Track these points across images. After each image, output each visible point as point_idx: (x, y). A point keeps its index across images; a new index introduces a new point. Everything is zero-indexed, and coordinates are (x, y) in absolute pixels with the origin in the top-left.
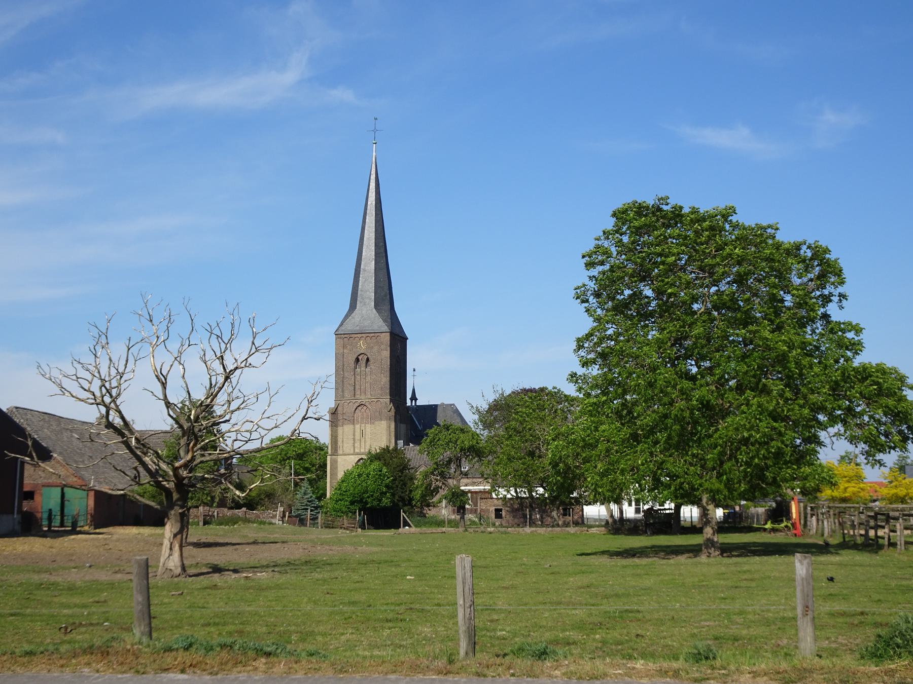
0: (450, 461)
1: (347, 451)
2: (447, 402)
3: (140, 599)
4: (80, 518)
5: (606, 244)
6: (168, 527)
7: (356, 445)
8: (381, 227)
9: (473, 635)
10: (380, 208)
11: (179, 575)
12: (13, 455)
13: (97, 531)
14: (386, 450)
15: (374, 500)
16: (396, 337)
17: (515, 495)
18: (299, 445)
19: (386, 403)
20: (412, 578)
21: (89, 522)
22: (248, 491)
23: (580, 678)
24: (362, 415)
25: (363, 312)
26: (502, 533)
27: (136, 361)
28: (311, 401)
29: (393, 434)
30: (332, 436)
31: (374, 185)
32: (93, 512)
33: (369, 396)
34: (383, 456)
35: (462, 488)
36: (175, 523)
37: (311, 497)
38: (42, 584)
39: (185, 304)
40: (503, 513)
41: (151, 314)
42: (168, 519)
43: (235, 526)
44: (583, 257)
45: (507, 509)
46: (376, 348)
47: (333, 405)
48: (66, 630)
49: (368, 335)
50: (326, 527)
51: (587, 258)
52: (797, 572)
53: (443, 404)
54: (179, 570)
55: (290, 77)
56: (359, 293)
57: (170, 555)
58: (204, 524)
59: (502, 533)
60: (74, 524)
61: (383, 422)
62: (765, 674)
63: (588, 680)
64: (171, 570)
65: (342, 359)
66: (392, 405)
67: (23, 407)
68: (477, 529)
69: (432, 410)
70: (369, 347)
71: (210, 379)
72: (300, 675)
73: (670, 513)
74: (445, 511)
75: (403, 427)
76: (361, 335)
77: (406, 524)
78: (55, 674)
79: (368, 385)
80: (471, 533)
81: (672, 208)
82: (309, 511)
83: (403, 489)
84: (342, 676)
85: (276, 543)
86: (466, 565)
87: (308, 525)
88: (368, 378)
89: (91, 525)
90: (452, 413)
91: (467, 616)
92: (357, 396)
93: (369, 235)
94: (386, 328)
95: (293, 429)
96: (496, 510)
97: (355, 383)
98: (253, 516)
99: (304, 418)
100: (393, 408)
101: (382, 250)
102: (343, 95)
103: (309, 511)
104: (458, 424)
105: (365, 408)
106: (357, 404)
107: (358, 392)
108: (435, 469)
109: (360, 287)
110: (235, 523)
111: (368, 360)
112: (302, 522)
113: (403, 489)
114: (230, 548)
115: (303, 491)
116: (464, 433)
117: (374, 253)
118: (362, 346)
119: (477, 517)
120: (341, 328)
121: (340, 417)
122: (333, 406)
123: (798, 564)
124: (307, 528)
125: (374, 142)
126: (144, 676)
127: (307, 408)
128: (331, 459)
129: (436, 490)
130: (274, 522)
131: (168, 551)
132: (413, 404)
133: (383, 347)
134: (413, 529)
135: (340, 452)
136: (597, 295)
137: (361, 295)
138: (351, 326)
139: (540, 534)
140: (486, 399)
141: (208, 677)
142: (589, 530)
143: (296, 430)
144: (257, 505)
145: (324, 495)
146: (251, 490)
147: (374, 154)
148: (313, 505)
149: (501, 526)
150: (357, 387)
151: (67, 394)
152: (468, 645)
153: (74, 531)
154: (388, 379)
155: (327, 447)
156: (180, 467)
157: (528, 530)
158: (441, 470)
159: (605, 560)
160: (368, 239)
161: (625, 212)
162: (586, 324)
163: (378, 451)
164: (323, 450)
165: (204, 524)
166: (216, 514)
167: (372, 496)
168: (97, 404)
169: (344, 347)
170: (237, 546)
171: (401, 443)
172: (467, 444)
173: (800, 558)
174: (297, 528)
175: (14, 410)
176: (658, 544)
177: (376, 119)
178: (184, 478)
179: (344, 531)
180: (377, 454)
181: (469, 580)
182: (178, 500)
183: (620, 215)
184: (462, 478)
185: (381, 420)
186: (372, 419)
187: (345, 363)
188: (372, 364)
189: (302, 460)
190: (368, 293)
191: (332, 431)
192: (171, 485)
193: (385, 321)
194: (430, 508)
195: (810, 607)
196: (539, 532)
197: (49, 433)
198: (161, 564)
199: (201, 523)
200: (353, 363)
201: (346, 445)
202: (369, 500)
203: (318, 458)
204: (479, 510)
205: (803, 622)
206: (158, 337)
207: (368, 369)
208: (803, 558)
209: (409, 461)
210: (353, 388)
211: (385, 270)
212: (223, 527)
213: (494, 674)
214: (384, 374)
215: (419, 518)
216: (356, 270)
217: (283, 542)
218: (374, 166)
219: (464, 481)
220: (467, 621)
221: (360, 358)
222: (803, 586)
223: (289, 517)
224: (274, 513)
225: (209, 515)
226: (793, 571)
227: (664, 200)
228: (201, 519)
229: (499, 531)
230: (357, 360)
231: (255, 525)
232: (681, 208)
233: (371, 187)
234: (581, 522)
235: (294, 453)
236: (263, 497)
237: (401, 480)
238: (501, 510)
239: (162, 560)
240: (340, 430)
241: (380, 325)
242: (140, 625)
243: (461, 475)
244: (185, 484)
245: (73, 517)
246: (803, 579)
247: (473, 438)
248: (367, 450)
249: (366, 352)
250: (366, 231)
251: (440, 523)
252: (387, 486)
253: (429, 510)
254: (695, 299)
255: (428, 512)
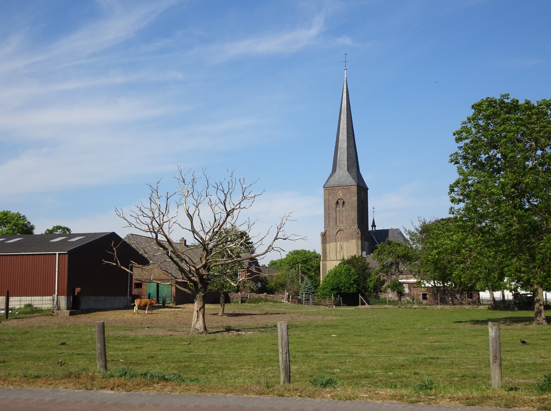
0: (392, 264)
1: (332, 258)
2: (394, 227)
3: (99, 346)
4: (167, 299)
5: (469, 125)
6: (196, 304)
7: (338, 255)
8: (350, 121)
9: (288, 371)
10: (349, 109)
11: (203, 332)
12: (107, 262)
13: (178, 306)
14: (354, 257)
15: (346, 288)
16: (361, 188)
17: (434, 285)
18: (304, 255)
19: (355, 229)
20: (335, 336)
21: (173, 301)
22: (238, 282)
23: (340, 399)
24: (341, 236)
25: (340, 173)
26: (423, 309)
27: (178, 206)
28: (280, 228)
29: (360, 248)
30: (323, 249)
31: (346, 95)
32: (175, 295)
33: (345, 225)
34: (352, 262)
35: (400, 281)
36: (200, 301)
37: (310, 286)
38: (119, 337)
39: (204, 171)
40: (428, 296)
41: (184, 178)
42: (196, 299)
43: (259, 304)
44: (454, 134)
45: (430, 293)
46: (348, 196)
47: (323, 230)
48: (61, 364)
49: (344, 187)
50: (314, 305)
51: (456, 136)
52: (490, 334)
53: (392, 229)
54: (202, 330)
55: (314, 31)
56: (338, 162)
57: (197, 320)
58: (242, 303)
59: (423, 309)
60: (164, 302)
61: (354, 240)
62: (458, 399)
63: (345, 400)
64: (198, 329)
65: (328, 202)
66: (359, 230)
67: (136, 234)
68: (406, 306)
69: (384, 233)
70: (345, 195)
71: (215, 216)
72: (177, 393)
73: (531, 297)
74: (391, 295)
75: (366, 243)
76: (339, 188)
77: (363, 304)
78: (43, 389)
79: (344, 218)
80: (403, 308)
81: (511, 101)
82: (304, 295)
83: (365, 281)
84: (200, 394)
85: (279, 314)
86: (283, 328)
87: (304, 303)
88: (344, 214)
89: (174, 303)
90: (398, 235)
91: (284, 359)
92: (338, 225)
93: (343, 126)
94: (354, 183)
95: (269, 245)
96: (423, 294)
97: (336, 217)
98: (270, 298)
99: (276, 239)
100: (360, 232)
101: (351, 135)
102: (345, 41)
103: (304, 295)
104: (401, 241)
105: (343, 232)
106: (338, 230)
107: (338, 222)
108: (382, 269)
109: (338, 158)
110: (260, 302)
111: (344, 203)
112: (300, 302)
113: (365, 281)
114: (249, 317)
115: (305, 283)
116: (400, 246)
117: (346, 137)
118: (340, 194)
119: (411, 299)
120: (328, 183)
121: (328, 239)
122: (323, 231)
123: (490, 329)
124: (303, 305)
125: (345, 69)
126: (90, 391)
127: (277, 233)
128: (323, 263)
129: (383, 282)
130: (282, 301)
131: (196, 318)
132: (374, 229)
133: (353, 194)
134: (367, 306)
135: (328, 259)
136: (464, 158)
137: (339, 163)
138: (333, 182)
139: (447, 309)
140: (414, 225)
141: (124, 393)
142: (478, 307)
143: (271, 246)
144: (275, 291)
145: (319, 285)
146: (240, 282)
147: (345, 76)
148: (311, 291)
149: (427, 304)
150: (338, 219)
151: (133, 226)
152: (285, 377)
153: (164, 306)
154: (356, 214)
155: (320, 256)
156: (200, 268)
157: (439, 307)
158: (386, 269)
159: (469, 326)
160: (343, 128)
161: (479, 105)
162: (454, 176)
163: (349, 258)
164: (318, 258)
165: (242, 303)
166: (249, 296)
167: (344, 285)
168: (151, 232)
169: (329, 195)
170: (253, 316)
171: (364, 253)
172: (401, 253)
173: (491, 325)
174: (296, 305)
175: (130, 236)
176: (118, 312)
177: (346, 54)
178: (203, 275)
179: (325, 307)
180: (349, 260)
181: (285, 337)
182: (201, 288)
183: (477, 107)
184: (399, 274)
185: (352, 239)
186: (347, 239)
187: (330, 205)
188: (346, 206)
189: (306, 264)
190: (343, 161)
191: (323, 246)
192: (196, 279)
193: (353, 178)
194: (382, 293)
195: (498, 357)
196: (446, 308)
197: (150, 249)
198: (192, 326)
199: (240, 302)
200: (335, 204)
201: (331, 255)
202: (343, 289)
203: (315, 263)
204: (412, 294)
205: (493, 366)
206: (188, 192)
207: (344, 208)
208: (493, 325)
209: (368, 264)
210: (335, 220)
211: (353, 147)
212: (252, 304)
213: (289, 395)
214: (354, 211)
215: (374, 299)
216: (335, 148)
217: (284, 314)
218: (345, 83)
219: (401, 276)
220: (284, 362)
221: (339, 201)
222: (493, 343)
223: (292, 298)
224: (283, 296)
225: (245, 297)
226: (487, 333)
227: (507, 96)
228: (240, 299)
229: (421, 307)
230: (337, 203)
231: (271, 303)
232: (517, 101)
233: (344, 96)
234: (479, 302)
235: (301, 260)
236: (278, 286)
237: (363, 276)
238: (426, 294)
239: (193, 324)
240: (328, 245)
241: (351, 181)
242: (99, 361)
243: (399, 273)
244: (204, 279)
245: (163, 298)
246: (493, 339)
247: (405, 249)
248: (341, 258)
249: (342, 198)
250: (341, 124)
251: (384, 302)
252: (354, 280)
253: (381, 294)
254: (527, 159)
255: (381, 295)
